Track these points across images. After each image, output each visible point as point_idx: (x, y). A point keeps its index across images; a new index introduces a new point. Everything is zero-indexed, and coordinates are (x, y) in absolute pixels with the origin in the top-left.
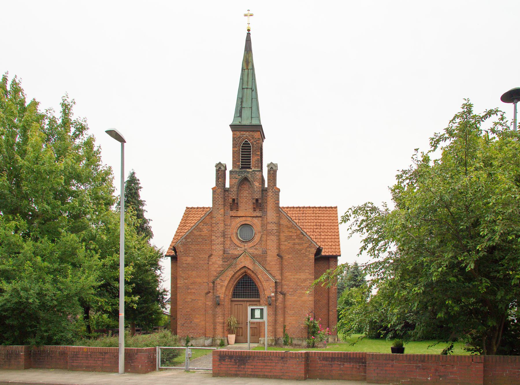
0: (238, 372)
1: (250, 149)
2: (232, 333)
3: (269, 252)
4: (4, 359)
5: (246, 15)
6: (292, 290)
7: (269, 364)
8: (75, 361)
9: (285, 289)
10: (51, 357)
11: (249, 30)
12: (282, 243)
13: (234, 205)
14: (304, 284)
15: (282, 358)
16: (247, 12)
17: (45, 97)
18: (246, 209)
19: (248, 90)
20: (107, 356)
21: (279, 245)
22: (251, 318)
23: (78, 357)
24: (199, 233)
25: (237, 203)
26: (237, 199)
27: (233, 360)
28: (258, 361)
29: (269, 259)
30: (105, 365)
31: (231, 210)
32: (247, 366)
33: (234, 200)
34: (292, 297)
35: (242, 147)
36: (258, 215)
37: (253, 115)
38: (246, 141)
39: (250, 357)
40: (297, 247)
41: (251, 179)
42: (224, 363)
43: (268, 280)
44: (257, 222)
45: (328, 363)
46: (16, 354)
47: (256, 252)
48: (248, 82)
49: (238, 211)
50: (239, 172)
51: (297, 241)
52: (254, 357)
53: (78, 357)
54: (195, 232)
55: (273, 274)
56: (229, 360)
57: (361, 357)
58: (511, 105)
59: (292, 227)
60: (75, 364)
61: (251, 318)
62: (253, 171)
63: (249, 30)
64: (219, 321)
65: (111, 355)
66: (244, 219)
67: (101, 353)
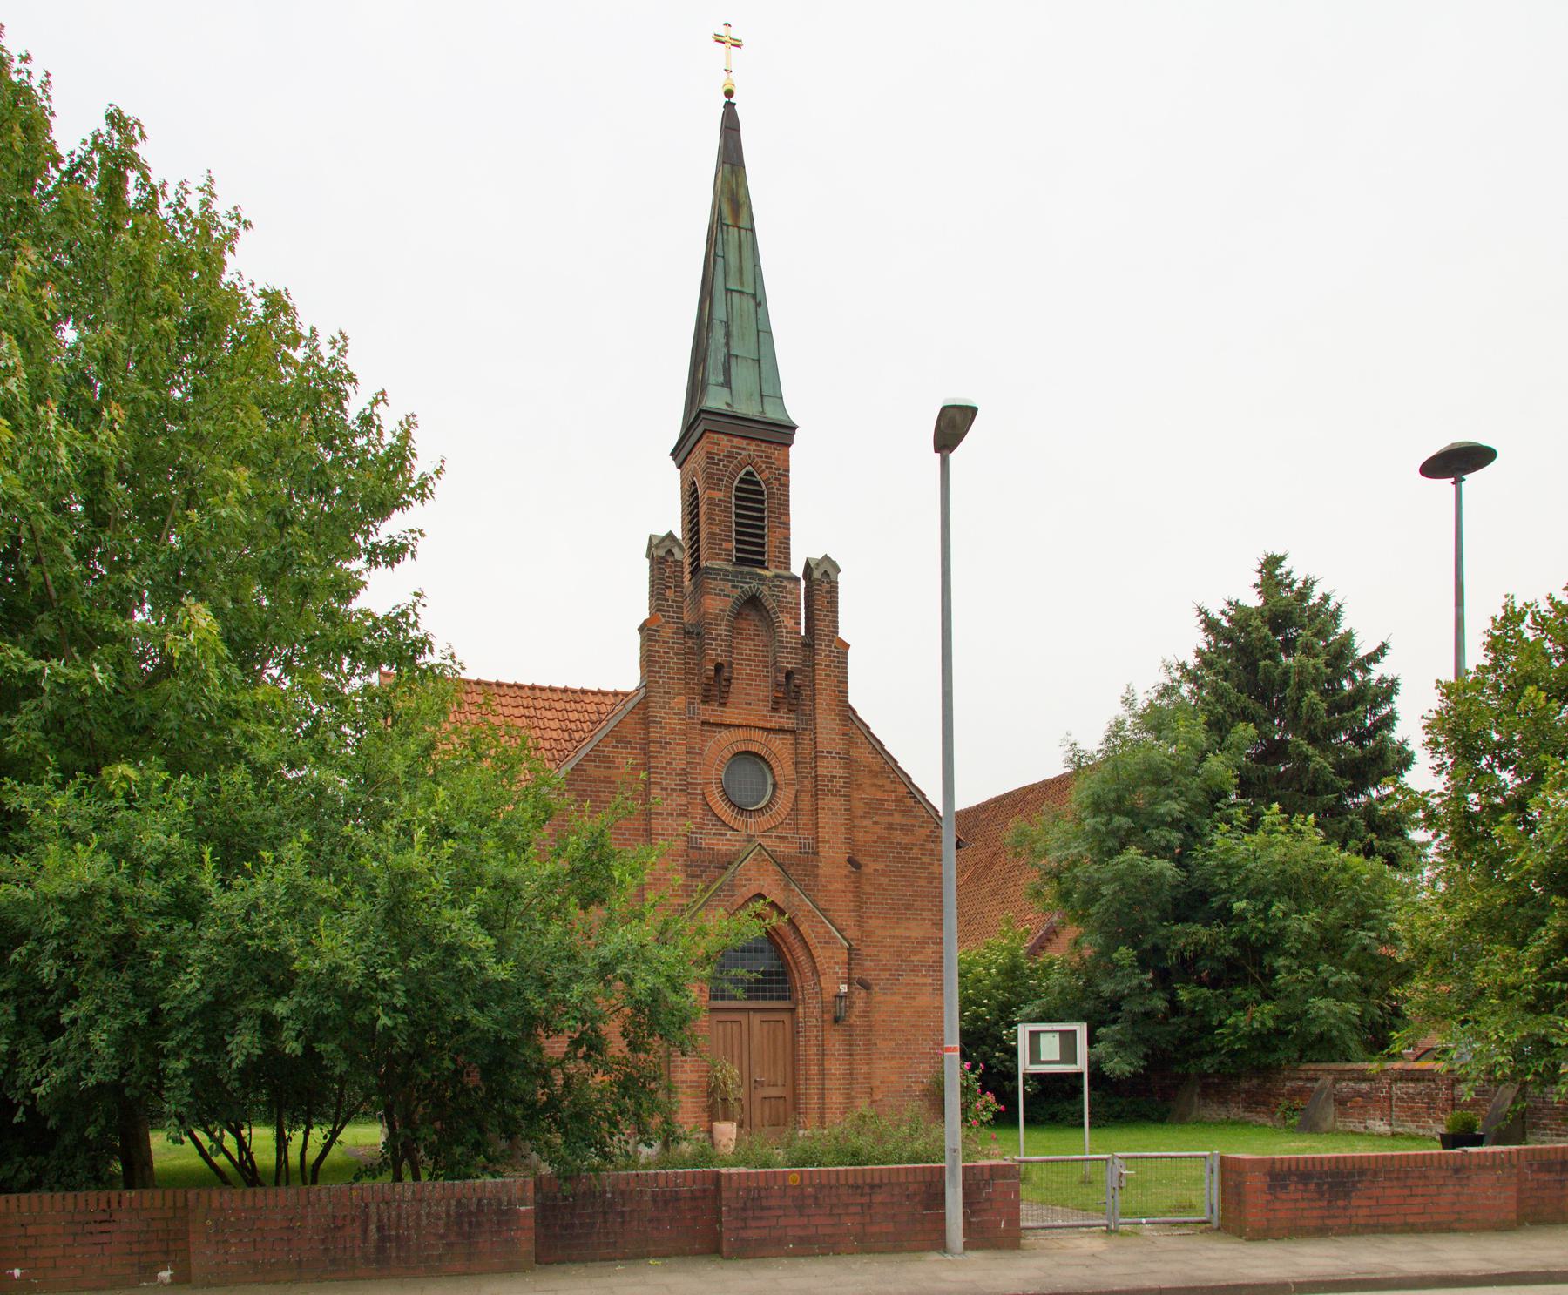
0: (1328, 1222)
3: (824, 850)
4: (442, 1237)
5: (719, 40)
6: (885, 975)
7: (1420, 1190)
8: (754, 1224)
9: (869, 969)
10: (622, 1214)
11: (729, 94)
12: (857, 822)
13: (717, 686)
14: (920, 957)
15: (1457, 1171)
16: (722, 31)
19: (744, 298)
20: (878, 1198)
21: (851, 829)
23: (762, 1208)
24: (602, 772)
25: (729, 680)
26: (731, 664)
27: (1312, 1187)
28: (1387, 1184)
29: (825, 870)
32: (1355, 1202)
34: (888, 998)
36: (786, 724)
38: (749, 473)
39: (1362, 1173)
40: (899, 836)
41: (770, 603)
42: (1283, 1195)
43: (828, 941)
44: (779, 748)
45: (1553, 1176)
46: (500, 1212)
47: (782, 848)
49: (723, 704)
50: (736, 574)
51: (897, 818)
52: (1375, 1174)
55: (838, 922)
56: (1300, 1186)
57: (877, 1181)
58: (1446, 484)
59: (883, 771)
60: (752, 1234)
62: (777, 576)
63: (729, 94)
64: (684, 1077)
65: (897, 1191)
66: (742, 733)
67: (856, 1187)
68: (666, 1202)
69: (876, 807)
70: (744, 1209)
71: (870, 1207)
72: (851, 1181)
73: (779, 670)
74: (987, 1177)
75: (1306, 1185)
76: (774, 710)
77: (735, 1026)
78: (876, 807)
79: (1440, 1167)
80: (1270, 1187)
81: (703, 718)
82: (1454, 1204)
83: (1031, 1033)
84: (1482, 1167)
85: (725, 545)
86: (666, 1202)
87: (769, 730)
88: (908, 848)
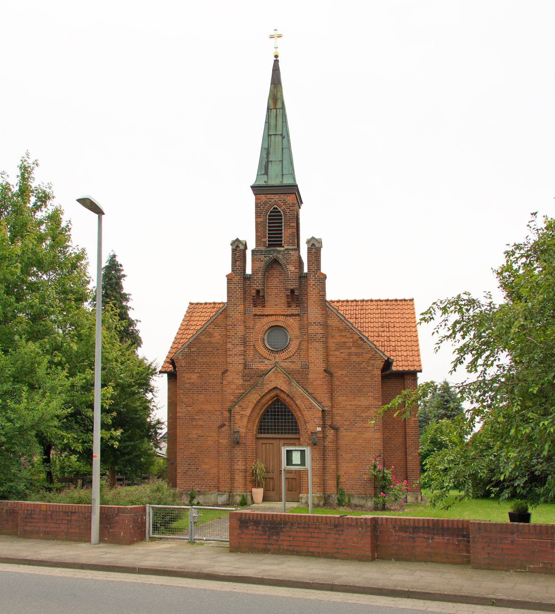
0: (268, 546)
1: (281, 219)
3: (312, 366)
5: (272, 37)
6: (348, 423)
7: (316, 535)
8: (29, 524)
11: (276, 56)
12: (331, 353)
13: (259, 298)
14: (367, 414)
15: (336, 526)
16: (273, 33)
18: (276, 304)
19: (277, 137)
20: (74, 518)
21: (327, 356)
23: (32, 518)
25: (263, 296)
26: (263, 290)
27: (260, 528)
28: (298, 530)
29: (311, 376)
30: (72, 531)
31: (255, 307)
33: (258, 292)
34: (349, 434)
35: (269, 216)
39: (286, 523)
40: (354, 358)
41: (283, 261)
42: (246, 531)
45: (408, 535)
47: (293, 366)
48: (276, 126)
49: (264, 307)
50: (266, 251)
51: (353, 350)
52: (292, 524)
53: (32, 518)
54: (202, 338)
55: (319, 399)
56: (255, 528)
57: (74, 511)
59: (345, 329)
60: (28, 529)
61: (287, 465)
62: (286, 249)
63: (276, 56)
64: (238, 467)
66: (273, 318)
68: (10, 514)
69: (342, 346)
70: (26, 518)
71: (71, 521)
72: (64, 510)
73: (287, 290)
74: (116, 512)
75: (257, 527)
76: (289, 306)
77: (271, 446)
78: (342, 346)
79: (327, 524)
80: (240, 527)
81: (254, 313)
82: (335, 544)
83: (287, 451)
84: (350, 526)
85: (263, 240)
86: (10, 514)
87: (287, 315)
88: (359, 364)
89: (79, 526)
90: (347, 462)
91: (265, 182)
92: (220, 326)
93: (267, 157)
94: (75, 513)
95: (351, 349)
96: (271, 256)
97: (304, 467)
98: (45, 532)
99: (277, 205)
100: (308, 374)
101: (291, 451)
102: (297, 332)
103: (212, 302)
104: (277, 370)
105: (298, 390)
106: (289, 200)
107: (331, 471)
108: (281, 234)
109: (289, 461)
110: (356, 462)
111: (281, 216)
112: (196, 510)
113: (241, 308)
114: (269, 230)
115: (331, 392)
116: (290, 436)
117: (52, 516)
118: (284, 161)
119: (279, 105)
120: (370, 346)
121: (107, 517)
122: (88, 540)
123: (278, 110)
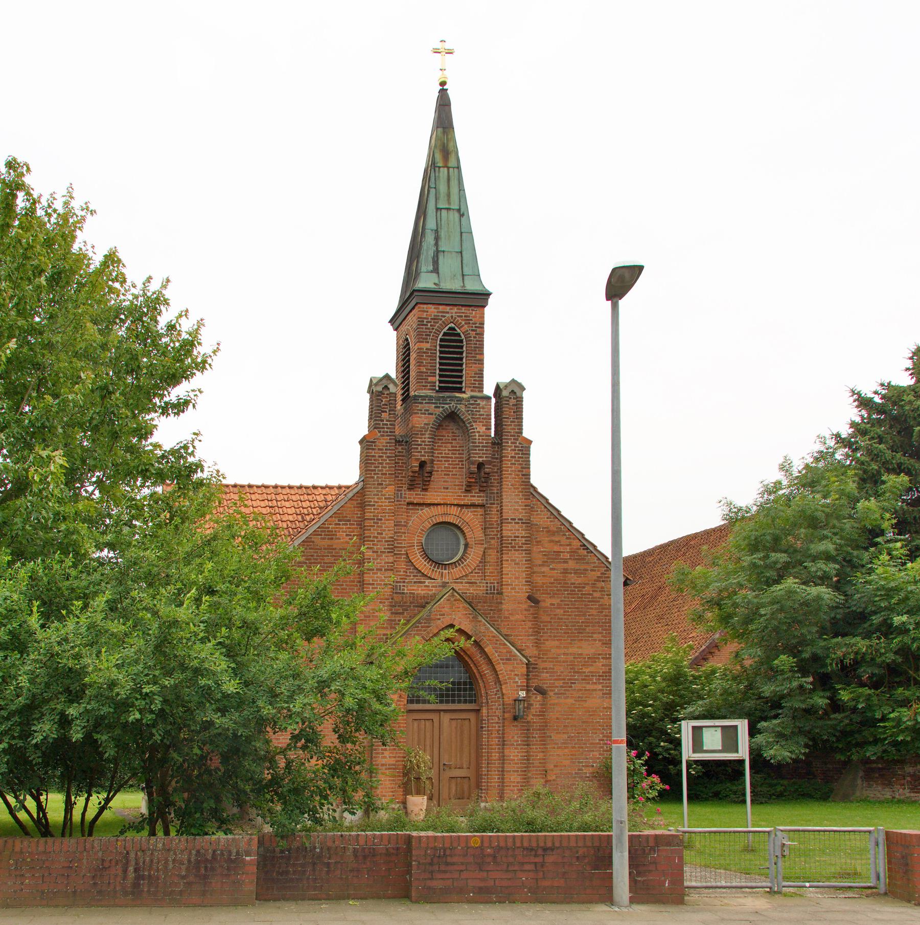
1: (462, 347)
2: (418, 793)
3: (507, 591)
4: (183, 877)
5: (436, 51)
8: (439, 876)
9: (544, 679)
11: (443, 84)
12: (535, 569)
13: (421, 477)
14: (591, 669)
16: (439, 46)
17: (45, 184)
18: (446, 489)
19: (451, 212)
20: (550, 859)
21: (531, 574)
22: (694, 752)
23: (447, 864)
24: (326, 543)
26: (432, 461)
30: (547, 883)
31: (409, 489)
33: (422, 464)
34: (562, 701)
35: (441, 340)
36: (477, 500)
37: (467, 271)
40: (573, 578)
41: (466, 417)
43: (510, 658)
46: (230, 860)
47: (472, 590)
48: (449, 195)
49: (426, 490)
50: (438, 399)
51: (571, 564)
53: (447, 864)
54: (317, 539)
55: (519, 644)
57: (549, 844)
59: (559, 531)
60: (437, 884)
61: (694, 752)
62: (472, 397)
63: (443, 84)
64: (384, 761)
65: (567, 853)
68: (365, 857)
70: (431, 864)
73: (473, 463)
74: (651, 844)
85: (430, 379)
86: (365, 857)
87: (462, 506)
88: (581, 587)
89: (564, 873)
90: (559, 748)
91: (435, 284)
92: (349, 521)
93: (436, 244)
94: (552, 849)
95: (567, 562)
96: (447, 406)
97: (735, 755)
98: (481, 888)
99: (441, 322)
100: (501, 603)
101: (701, 728)
102: (479, 534)
103: (246, 483)
104: (453, 596)
105: (488, 629)
106: (474, 317)
107: (536, 763)
108: (461, 371)
109: (698, 745)
110: (573, 747)
111: (461, 341)
112: (784, 834)
113: (390, 490)
114: (441, 364)
115: (537, 631)
116: (462, 706)
117: (495, 857)
118: (464, 253)
119: (452, 163)
120: (599, 559)
121: (640, 851)
122: (606, 896)
123: (451, 170)
